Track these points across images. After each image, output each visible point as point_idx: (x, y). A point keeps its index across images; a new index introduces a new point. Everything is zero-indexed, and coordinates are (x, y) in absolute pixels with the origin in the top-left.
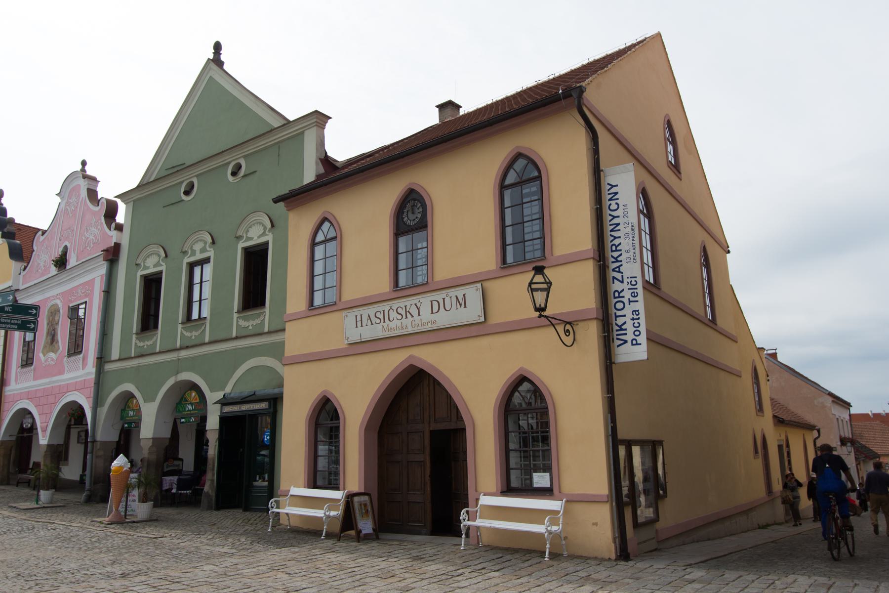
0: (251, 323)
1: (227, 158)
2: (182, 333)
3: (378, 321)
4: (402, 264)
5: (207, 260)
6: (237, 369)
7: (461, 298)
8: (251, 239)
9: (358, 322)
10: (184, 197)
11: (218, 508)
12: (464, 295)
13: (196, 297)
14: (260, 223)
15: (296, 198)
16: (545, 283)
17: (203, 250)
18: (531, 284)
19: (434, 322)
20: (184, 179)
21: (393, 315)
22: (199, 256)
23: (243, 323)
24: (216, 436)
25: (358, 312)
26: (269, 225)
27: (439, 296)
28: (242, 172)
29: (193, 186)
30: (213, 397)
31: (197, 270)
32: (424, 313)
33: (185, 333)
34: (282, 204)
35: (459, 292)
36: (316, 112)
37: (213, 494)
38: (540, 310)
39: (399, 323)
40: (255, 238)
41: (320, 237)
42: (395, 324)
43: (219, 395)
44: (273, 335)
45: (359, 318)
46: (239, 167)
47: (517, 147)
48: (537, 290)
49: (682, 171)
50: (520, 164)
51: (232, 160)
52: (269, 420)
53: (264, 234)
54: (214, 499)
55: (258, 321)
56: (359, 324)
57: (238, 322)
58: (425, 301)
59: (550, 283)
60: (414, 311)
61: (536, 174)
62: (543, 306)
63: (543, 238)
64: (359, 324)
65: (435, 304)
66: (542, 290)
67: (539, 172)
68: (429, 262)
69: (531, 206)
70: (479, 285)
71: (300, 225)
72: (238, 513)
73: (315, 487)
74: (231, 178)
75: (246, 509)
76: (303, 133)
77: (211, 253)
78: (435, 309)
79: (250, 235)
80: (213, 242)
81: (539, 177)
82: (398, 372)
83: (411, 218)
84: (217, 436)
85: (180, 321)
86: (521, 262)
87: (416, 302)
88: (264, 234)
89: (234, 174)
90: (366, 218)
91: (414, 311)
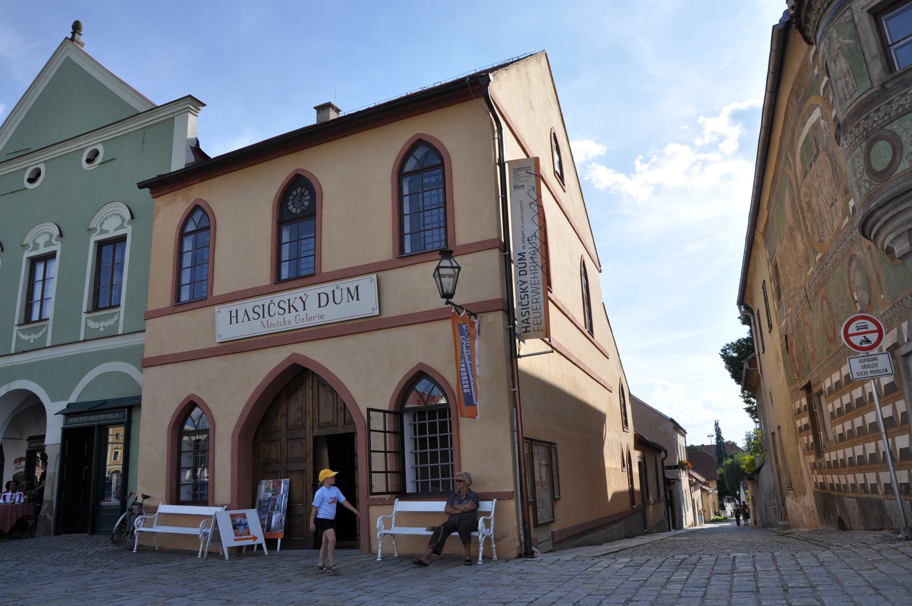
0: (103, 324)
1: (81, 143)
2: (18, 337)
3: (256, 316)
4: (285, 255)
5: (52, 256)
6: (85, 374)
7: (353, 290)
8: (107, 232)
9: (233, 318)
10: (27, 185)
11: (57, 532)
12: (357, 287)
13: (37, 295)
14: (118, 215)
15: (161, 185)
16: (452, 267)
17: (48, 244)
18: (438, 268)
19: (322, 317)
20: (29, 165)
21: (274, 309)
22: (42, 250)
23: (92, 325)
24: (58, 450)
25: (233, 306)
26: (128, 217)
27: (328, 288)
28: (99, 159)
29: (39, 174)
30: (54, 409)
31: (40, 268)
32: (308, 306)
33: (21, 335)
34: (147, 190)
35: (351, 283)
36: (190, 96)
37: (51, 518)
38: (447, 296)
39: (281, 318)
40: (111, 231)
41: (191, 227)
42: (277, 318)
43: (62, 405)
44: (128, 336)
45: (234, 314)
46: (96, 153)
47: (418, 134)
48: (444, 276)
49: (566, 183)
50: (420, 153)
51: (88, 145)
52: (121, 430)
53: (122, 226)
54: (52, 523)
55: (111, 322)
56: (234, 320)
57: (87, 322)
58: (311, 293)
59: (459, 268)
60: (299, 305)
61: (438, 162)
62: (450, 290)
63: (446, 227)
64: (234, 320)
65: (323, 297)
66: (449, 276)
67: (442, 160)
68: (316, 254)
69: (431, 196)
70: (374, 276)
71: (171, 211)
72: (83, 536)
73: (178, 502)
74: (85, 166)
75: (93, 532)
76: (173, 118)
77: (57, 247)
78: (323, 303)
79: (104, 227)
80: (61, 235)
81: (442, 165)
82: (280, 371)
83: (298, 208)
84: (58, 451)
85: (16, 322)
86: (420, 254)
87: (302, 295)
88: (122, 226)
89: (89, 161)
90: (244, 217)
91: (299, 305)
